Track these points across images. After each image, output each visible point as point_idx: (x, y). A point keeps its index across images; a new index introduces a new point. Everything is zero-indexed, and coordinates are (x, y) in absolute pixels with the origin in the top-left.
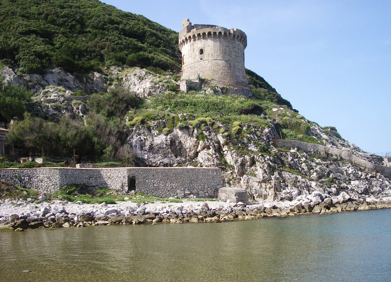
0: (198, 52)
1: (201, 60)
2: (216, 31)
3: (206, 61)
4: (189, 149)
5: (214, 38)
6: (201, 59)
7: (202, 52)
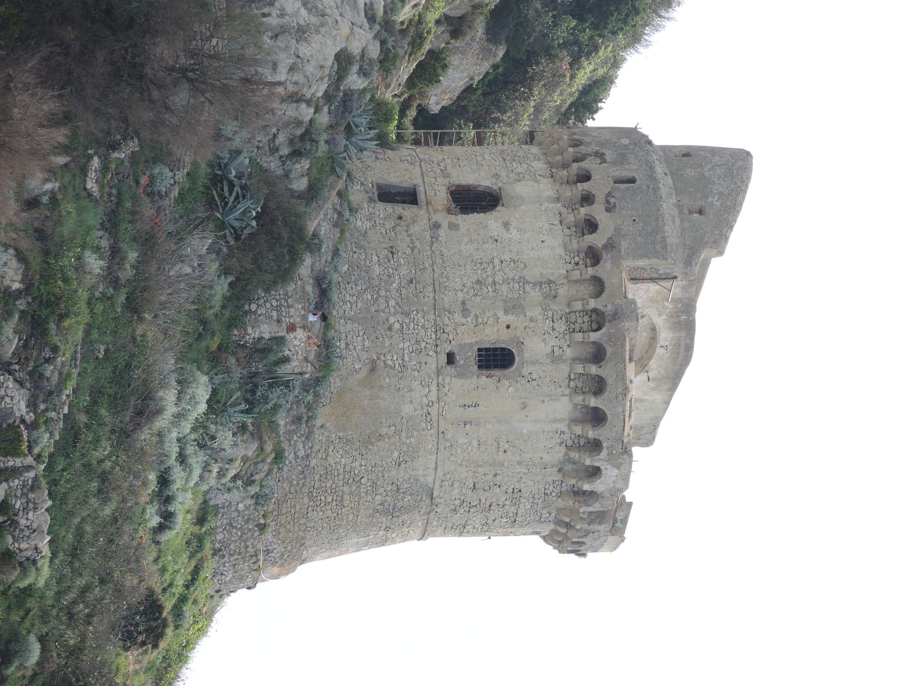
1: (443, 359)
3: (434, 388)
5: (566, 437)
6: (451, 359)
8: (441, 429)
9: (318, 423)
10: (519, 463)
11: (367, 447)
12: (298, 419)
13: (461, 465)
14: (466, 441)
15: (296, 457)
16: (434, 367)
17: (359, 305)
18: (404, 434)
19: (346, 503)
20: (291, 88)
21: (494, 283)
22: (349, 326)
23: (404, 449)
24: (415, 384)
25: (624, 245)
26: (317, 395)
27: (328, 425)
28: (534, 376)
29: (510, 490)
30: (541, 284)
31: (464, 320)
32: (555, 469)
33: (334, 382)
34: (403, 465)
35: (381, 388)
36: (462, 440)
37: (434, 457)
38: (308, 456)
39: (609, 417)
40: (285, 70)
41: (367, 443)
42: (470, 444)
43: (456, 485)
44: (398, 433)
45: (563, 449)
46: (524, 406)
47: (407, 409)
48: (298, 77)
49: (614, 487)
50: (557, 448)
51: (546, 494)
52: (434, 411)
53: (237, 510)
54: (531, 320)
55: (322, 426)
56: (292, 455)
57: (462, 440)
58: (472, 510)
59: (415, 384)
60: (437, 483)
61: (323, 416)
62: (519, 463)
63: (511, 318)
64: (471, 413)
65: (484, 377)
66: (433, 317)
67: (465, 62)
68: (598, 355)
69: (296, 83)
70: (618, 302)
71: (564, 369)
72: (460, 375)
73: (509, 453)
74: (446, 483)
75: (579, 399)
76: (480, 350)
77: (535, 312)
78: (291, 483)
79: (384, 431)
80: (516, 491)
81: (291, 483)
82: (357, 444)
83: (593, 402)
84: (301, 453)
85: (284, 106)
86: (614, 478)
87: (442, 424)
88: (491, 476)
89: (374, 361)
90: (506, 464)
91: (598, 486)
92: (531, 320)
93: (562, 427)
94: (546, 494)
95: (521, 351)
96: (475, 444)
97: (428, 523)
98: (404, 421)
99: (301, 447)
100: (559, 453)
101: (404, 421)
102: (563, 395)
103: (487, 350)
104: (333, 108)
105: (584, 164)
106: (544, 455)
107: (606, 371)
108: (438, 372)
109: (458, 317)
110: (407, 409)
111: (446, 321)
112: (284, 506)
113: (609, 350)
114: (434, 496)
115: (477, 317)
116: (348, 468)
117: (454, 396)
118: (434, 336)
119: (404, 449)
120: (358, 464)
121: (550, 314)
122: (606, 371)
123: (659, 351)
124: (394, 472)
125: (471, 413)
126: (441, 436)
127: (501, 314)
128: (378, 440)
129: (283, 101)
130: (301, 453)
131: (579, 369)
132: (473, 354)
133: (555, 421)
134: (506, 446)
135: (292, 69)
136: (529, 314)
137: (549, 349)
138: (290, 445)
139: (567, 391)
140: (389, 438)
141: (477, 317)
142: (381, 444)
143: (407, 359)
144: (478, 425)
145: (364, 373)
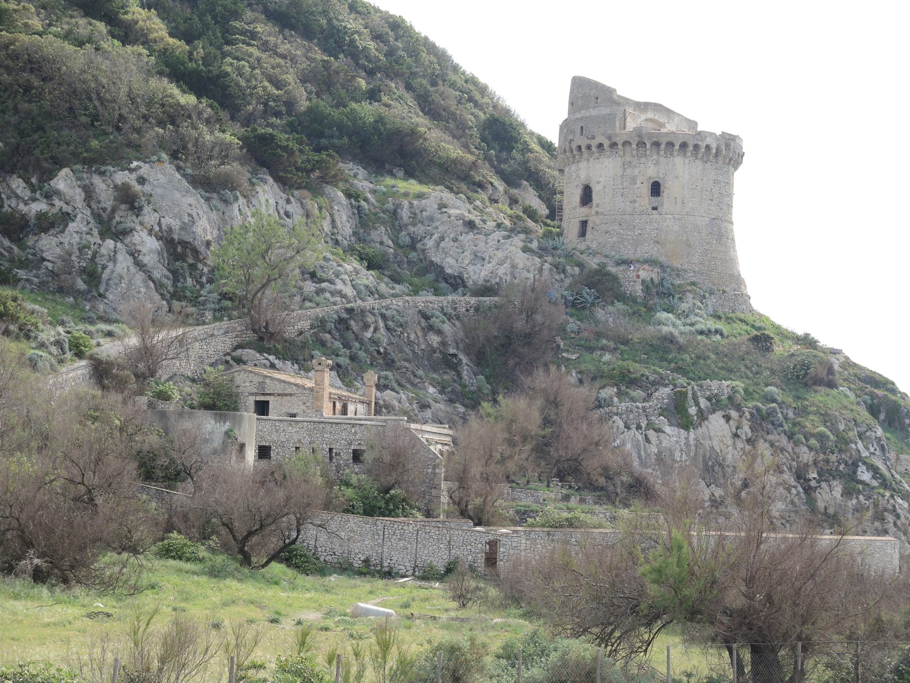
0: (646, 190)
1: (655, 211)
3: (667, 216)
4: (731, 468)
6: (655, 208)
7: (656, 189)
15: (694, 276)
19: (715, 256)
20: (536, 272)
22: (638, 252)
25: (609, 132)
26: (668, 267)
27: (681, 262)
33: (662, 259)
36: (691, 205)
41: (690, 246)
44: (686, 232)
45: (697, 161)
46: (677, 177)
47: (676, 228)
48: (532, 269)
52: (677, 217)
57: (691, 205)
59: (665, 224)
61: (677, 264)
63: (638, 182)
64: (679, 201)
68: (657, 144)
71: (662, 159)
72: (662, 204)
77: (636, 171)
79: (685, 239)
84: (692, 274)
87: (683, 213)
91: (714, 146)
93: (687, 161)
95: (653, 178)
107: (664, 141)
108: (660, 214)
109: (637, 205)
110: (676, 228)
113: (655, 139)
122: (664, 141)
125: (679, 201)
127: (636, 186)
130: (692, 274)
132: (653, 199)
133: (684, 164)
135: (528, 271)
136: (637, 174)
139: (672, 158)
145: (659, 247)
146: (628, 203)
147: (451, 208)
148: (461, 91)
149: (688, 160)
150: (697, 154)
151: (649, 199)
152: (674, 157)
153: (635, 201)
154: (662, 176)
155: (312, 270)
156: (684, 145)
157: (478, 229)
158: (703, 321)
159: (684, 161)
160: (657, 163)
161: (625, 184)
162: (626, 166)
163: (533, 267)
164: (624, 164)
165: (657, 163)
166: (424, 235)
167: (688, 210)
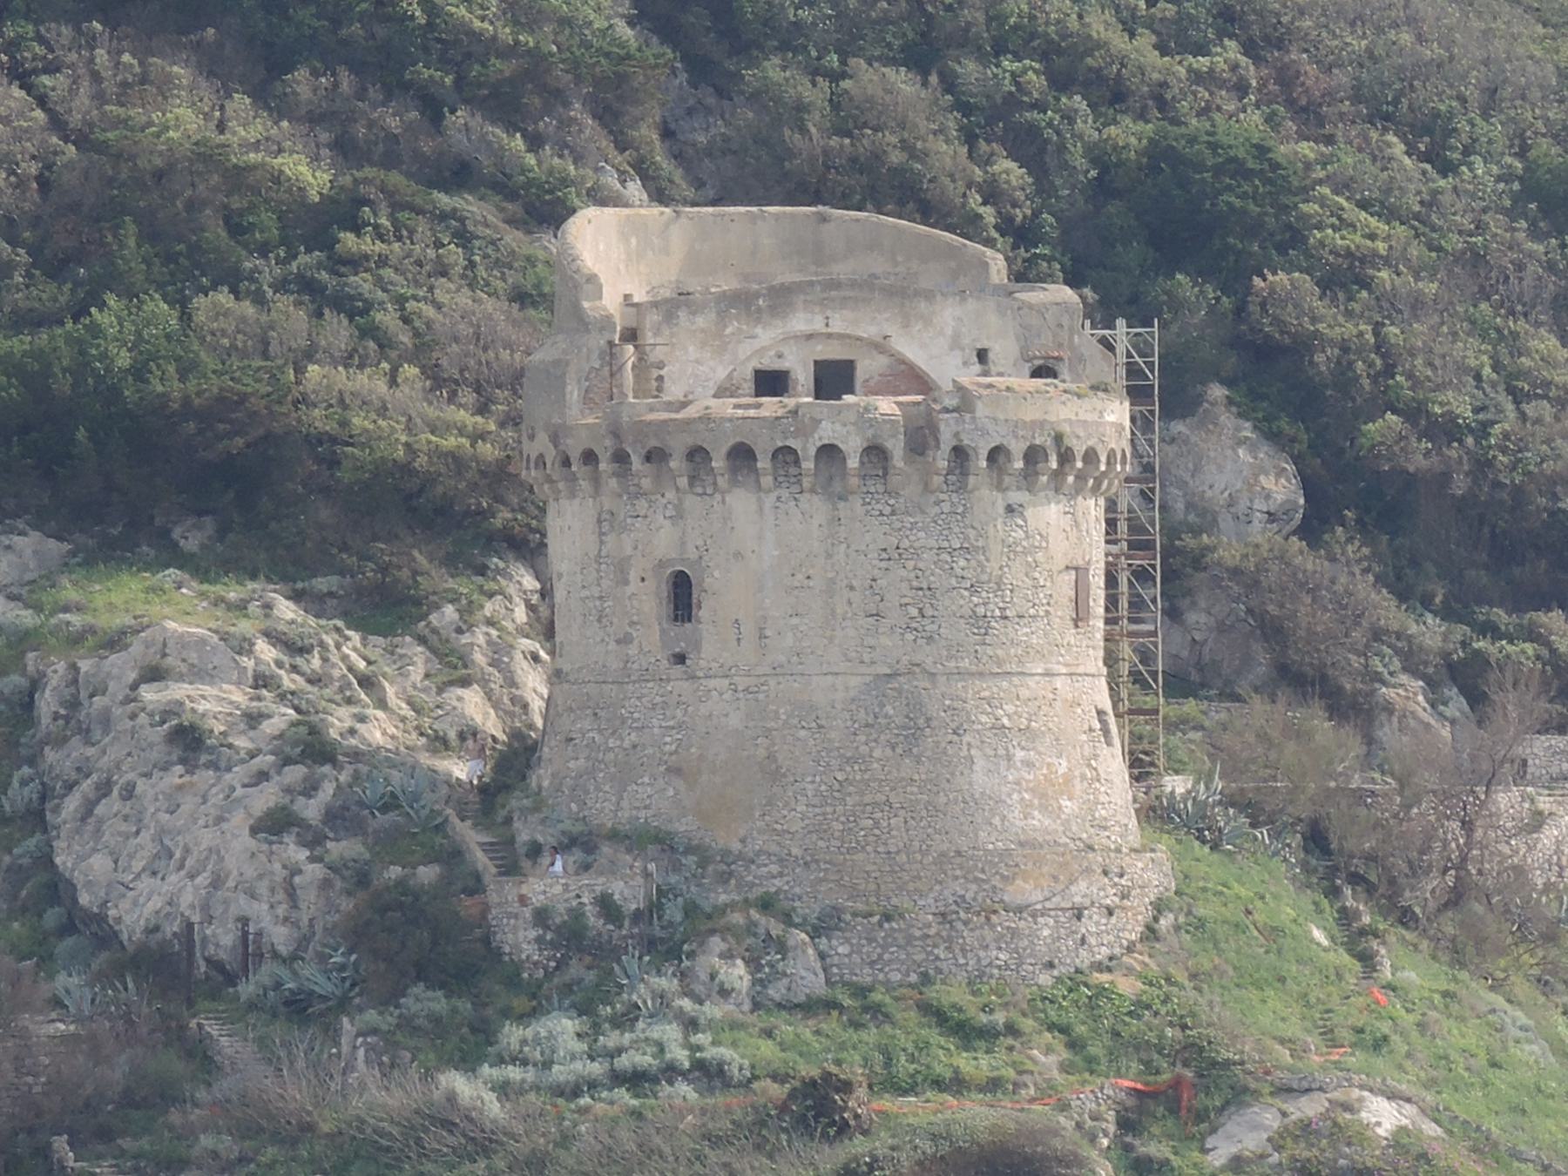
0: (649, 600)
2: (791, 443)
3: (712, 683)
5: (785, 493)
6: (680, 659)
8: (769, 670)
9: (736, 846)
10: (829, 556)
11: (784, 775)
12: (724, 878)
13: (831, 640)
14: (790, 634)
15: (781, 875)
16: (686, 685)
17: (607, 788)
18: (772, 724)
19: (881, 798)
20: (281, 896)
21: (601, 598)
22: (625, 804)
23: (795, 721)
24: (703, 710)
25: (556, 420)
26: (689, 850)
27: (742, 832)
28: (700, 542)
29: (884, 564)
30: (602, 534)
31: (636, 642)
32: (841, 505)
33: (684, 826)
34: (823, 722)
35: (701, 757)
36: (789, 640)
37: (815, 678)
38: (781, 860)
39: (738, 439)
40: (255, 905)
41: (776, 775)
42: (796, 627)
43: (870, 641)
44: (767, 733)
46: (738, 555)
47: (735, 721)
48: (263, 888)
49: (853, 424)
50: (804, 505)
51: (893, 513)
52: (742, 682)
53: (848, 956)
54: (636, 548)
55: (743, 841)
56: (777, 882)
57: (789, 640)
58: (929, 612)
59: (703, 710)
60: (863, 669)
61: (726, 839)
62: (829, 556)
63: (633, 576)
64: (748, 629)
65: (701, 613)
66: (630, 686)
67: (1212, 454)
68: (697, 455)
69: (273, 890)
70: (602, 432)
71: (690, 501)
72: (697, 646)
73: (811, 572)
74: (866, 658)
75: (722, 482)
76: (676, 619)
77: (627, 541)
78: (821, 880)
79: (762, 753)
80: (884, 555)
81: (821, 880)
82: (775, 789)
83: (808, 465)
84: (774, 868)
85: (303, 906)
86: (838, 427)
87: (760, 671)
88: (852, 594)
89: (669, 770)
90: (830, 575)
92: (636, 548)
93: (770, 500)
94: (893, 513)
95: (671, 562)
96: (795, 621)
97: (981, 674)
98: (751, 724)
99: (765, 870)
100: (816, 506)
101: (751, 724)
102: (723, 501)
103: (676, 608)
104: (331, 835)
105: (575, 455)
106: (815, 522)
107: (678, 445)
108: (693, 677)
109: (633, 650)
110: (735, 721)
111: (636, 666)
112: (862, 887)
113: (653, 443)
114: (888, 671)
115: (632, 624)
116: (816, 801)
117: (725, 654)
118: (650, 685)
119: (795, 721)
120: (810, 786)
121: (629, 521)
122: (678, 445)
123: (837, 326)
124: (833, 735)
125: (748, 629)
126: (778, 670)
127: (630, 589)
128: (776, 761)
129: (295, 906)
130: (774, 868)
131: (767, 481)
132: (676, 630)
133: (761, 509)
134: (800, 576)
135: (253, 896)
136: (629, 551)
137: (667, 523)
138: (761, 885)
139: (718, 497)
140: (774, 744)
141: (632, 624)
142: (780, 757)
143: (671, 723)
144: (765, 618)
145: (680, 784)
146: (612, 646)
147: (181, 678)
148: (834, 284)
149: (773, 496)
150: (1001, 472)
151: (663, 631)
152: (723, 493)
153: (625, 640)
154: (692, 554)
155: (609, 825)
156: (997, 455)
157: (211, 750)
158: (530, 1075)
159: (759, 500)
160: (678, 516)
161: (605, 583)
162: (606, 527)
163: (265, 883)
164: (599, 521)
165: (678, 516)
166: (74, 776)
167: (782, 659)
